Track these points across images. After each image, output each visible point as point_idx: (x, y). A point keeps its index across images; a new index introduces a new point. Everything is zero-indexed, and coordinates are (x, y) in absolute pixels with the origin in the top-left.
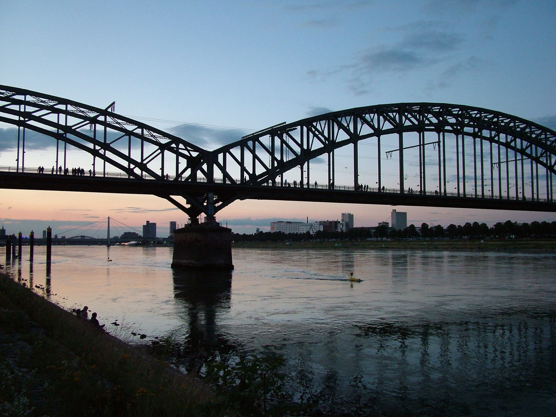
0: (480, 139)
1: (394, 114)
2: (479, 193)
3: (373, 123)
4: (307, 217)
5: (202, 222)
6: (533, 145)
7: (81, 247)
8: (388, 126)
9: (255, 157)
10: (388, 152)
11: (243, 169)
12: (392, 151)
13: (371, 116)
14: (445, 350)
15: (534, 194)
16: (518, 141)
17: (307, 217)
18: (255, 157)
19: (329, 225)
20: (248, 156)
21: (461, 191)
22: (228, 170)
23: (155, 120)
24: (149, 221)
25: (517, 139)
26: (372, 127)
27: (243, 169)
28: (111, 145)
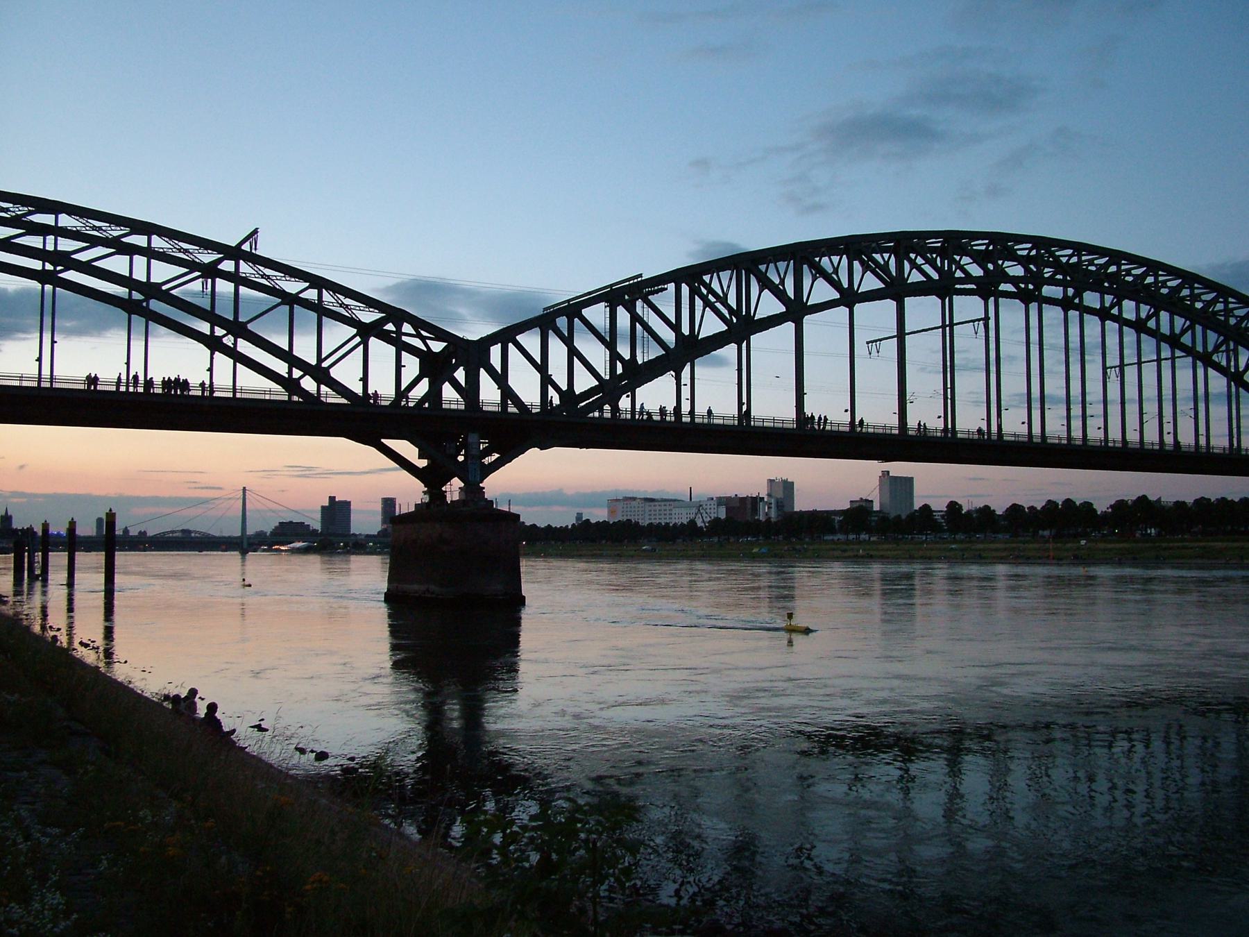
0: (1078, 313)
1: (886, 256)
2: (1077, 433)
3: (838, 277)
4: (691, 488)
5: (454, 499)
6: (1197, 326)
7: (183, 555)
8: (871, 283)
9: (573, 353)
10: (872, 342)
11: (546, 381)
12: (880, 340)
13: (833, 260)
14: (999, 786)
15: (1200, 436)
16: (1164, 316)
17: (691, 488)
18: (573, 353)
19: (738, 505)
20: (557, 350)
21: (1036, 430)
22: (512, 382)
23: (349, 270)
24: (335, 497)
25: (1162, 313)
26: (836, 285)
27: (546, 381)
28: (248, 325)
